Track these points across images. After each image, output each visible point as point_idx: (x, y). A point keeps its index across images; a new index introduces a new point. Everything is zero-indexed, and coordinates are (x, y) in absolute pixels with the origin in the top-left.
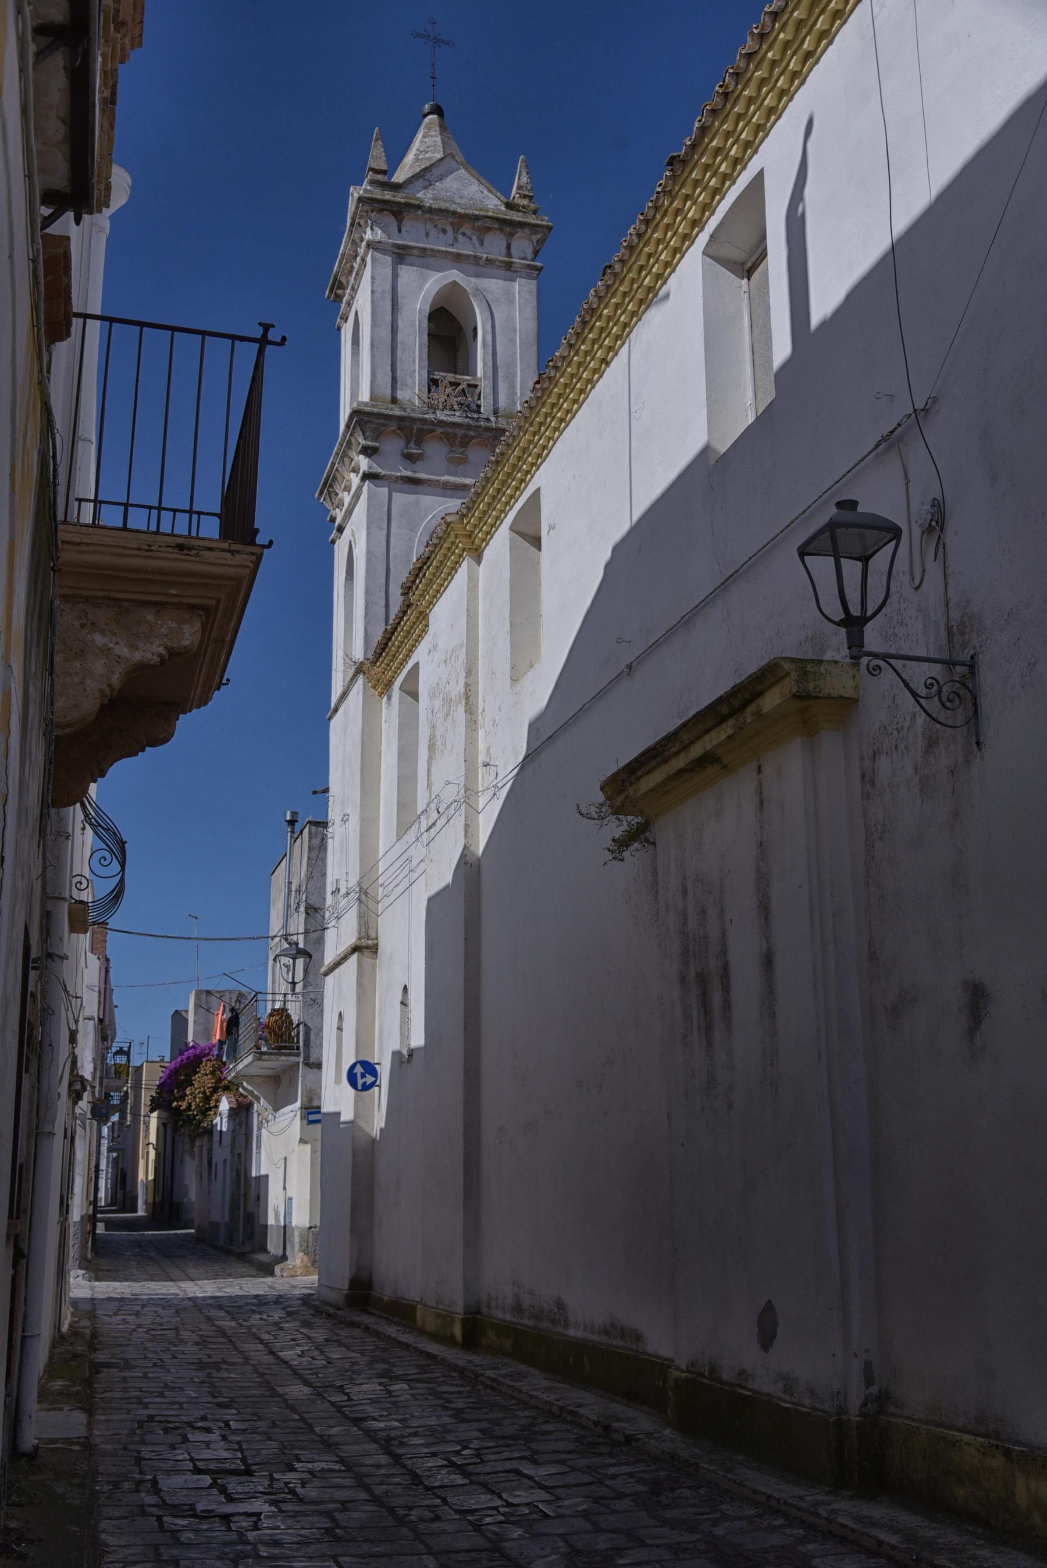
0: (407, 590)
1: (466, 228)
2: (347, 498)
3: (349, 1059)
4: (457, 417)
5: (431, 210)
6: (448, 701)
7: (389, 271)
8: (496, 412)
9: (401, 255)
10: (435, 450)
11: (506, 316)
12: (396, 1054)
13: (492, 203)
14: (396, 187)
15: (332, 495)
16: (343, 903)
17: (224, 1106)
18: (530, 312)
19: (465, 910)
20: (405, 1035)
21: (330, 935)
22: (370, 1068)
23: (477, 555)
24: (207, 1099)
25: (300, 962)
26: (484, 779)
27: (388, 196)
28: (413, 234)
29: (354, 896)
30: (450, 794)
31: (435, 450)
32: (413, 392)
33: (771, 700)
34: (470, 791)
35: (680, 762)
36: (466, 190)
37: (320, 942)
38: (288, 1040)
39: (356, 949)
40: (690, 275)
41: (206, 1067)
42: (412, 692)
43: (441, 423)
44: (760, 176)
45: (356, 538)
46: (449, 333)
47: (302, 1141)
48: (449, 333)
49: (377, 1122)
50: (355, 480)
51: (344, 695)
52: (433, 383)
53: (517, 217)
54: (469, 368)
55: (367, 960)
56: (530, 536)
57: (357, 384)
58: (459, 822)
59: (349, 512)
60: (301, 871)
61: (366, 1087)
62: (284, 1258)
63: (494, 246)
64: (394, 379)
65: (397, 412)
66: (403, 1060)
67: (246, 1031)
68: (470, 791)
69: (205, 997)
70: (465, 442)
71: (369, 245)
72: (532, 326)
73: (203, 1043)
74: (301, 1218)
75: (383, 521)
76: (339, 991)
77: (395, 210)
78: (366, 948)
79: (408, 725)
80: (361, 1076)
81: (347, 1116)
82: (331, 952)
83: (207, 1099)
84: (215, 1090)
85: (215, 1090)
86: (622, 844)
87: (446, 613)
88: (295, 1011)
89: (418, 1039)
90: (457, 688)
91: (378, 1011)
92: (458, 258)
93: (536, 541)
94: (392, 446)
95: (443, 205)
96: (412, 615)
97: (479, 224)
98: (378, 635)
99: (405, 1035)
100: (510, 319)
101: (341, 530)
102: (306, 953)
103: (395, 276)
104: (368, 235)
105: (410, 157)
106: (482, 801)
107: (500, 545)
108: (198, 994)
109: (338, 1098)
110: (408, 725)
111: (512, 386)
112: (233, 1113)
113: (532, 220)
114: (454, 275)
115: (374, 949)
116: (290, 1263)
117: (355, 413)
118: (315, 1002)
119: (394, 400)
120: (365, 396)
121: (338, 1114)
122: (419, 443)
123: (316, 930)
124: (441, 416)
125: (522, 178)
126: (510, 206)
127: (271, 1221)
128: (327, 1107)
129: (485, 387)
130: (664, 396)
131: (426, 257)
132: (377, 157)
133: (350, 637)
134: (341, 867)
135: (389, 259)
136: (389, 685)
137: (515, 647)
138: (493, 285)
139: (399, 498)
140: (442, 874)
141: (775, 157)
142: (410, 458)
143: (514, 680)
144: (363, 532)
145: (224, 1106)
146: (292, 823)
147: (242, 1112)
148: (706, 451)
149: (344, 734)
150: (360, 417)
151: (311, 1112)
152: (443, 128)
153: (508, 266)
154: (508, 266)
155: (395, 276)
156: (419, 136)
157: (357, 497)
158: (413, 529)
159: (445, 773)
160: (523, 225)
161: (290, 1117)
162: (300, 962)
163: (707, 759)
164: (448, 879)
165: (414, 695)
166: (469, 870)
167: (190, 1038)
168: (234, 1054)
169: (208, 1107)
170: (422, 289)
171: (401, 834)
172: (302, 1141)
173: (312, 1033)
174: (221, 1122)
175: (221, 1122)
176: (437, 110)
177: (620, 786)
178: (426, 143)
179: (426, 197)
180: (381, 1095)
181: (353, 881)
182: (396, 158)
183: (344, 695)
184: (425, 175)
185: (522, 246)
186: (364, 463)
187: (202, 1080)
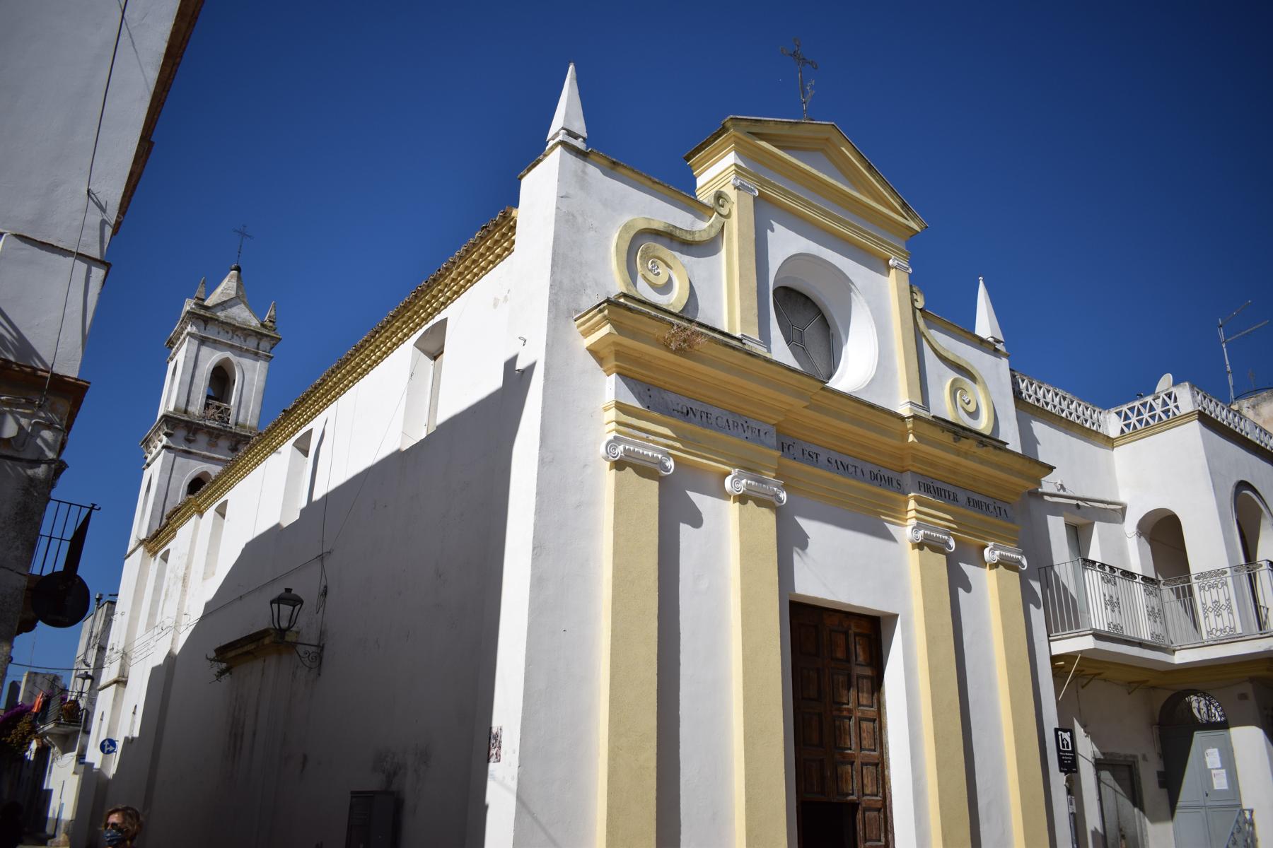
0: (169, 518)
1: (239, 333)
2: (155, 452)
3: (103, 737)
4: (215, 425)
5: (222, 322)
6: (176, 576)
7: (195, 348)
8: (236, 424)
9: (203, 341)
10: (202, 439)
11: (251, 378)
12: (126, 738)
13: (254, 323)
14: (207, 308)
15: (147, 446)
16: (114, 656)
17: (34, 746)
18: (263, 377)
19: (165, 678)
20: (132, 730)
21: (105, 671)
22: (112, 743)
23: (201, 514)
24: (24, 737)
25: (88, 682)
26: (185, 620)
27: (202, 312)
28: (211, 333)
29: (120, 655)
30: (169, 622)
31: (202, 439)
32: (197, 407)
33: (267, 641)
34: (177, 623)
35: (240, 651)
36: (242, 314)
37: (99, 677)
38: (75, 720)
39: (116, 682)
40: (288, 448)
41: (27, 718)
42: (165, 558)
43: (207, 427)
44: (311, 431)
45: (154, 472)
46: (221, 379)
47: (75, 773)
48: (221, 379)
49: (112, 771)
50: (160, 445)
51: (134, 550)
52: (207, 406)
53: (265, 332)
54: (228, 400)
55: (121, 689)
56: (221, 512)
57: (168, 402)
58: (170, 636)
59: (154, 459)
60: (99, 626)
61: (109, 752)
62: (54, 836)
63: (251, 344)
64: (188, 401)
65: (186, 418)
66: (129, 742)
67: (54, 706)
68: (177, 623)
69: (32, 676)
70: (218, 437)
71: (188, 334)
72: (262, 384)
73: (27, 704)
74: (68, 814)
75: (169, 471)
76: (105, 700)
77: (204, 317)
78: (121, 682)
79: (160, 575)
80: (107, 746)
81: (97, 766)
82: (104, 680)
83: (24, 737)
84: (30, 732)
85: (30, 732)
86: (222, 673)
87: (185, 532)
88: (82, 704)
89: (136, 734)
90: (181, 574)
91: (119, 715)
92: (232, 347)
93: (223, 516)
94: (181, 433)
95: (229, 321)
96: (168, 529)
97: (246, 332)
98: (156, 527)
99: (132, 730)
100: (253, 379)
101: (148, 465)
102: (94, 679)
103: (198, 350)
104: (189, 329)
105: (219, 290)
106: (183, 628)
107: (210, 513)
108: (30, 674)
109: (94, 756)
110: (160, 575)
111: (247, 412)
112: (38, 750)
113: (272, 334)
114: (228, 354)
115: (125, 683)
116: (57, 839)
117: (164, 416)
118: (92, 702)
119: (186, 412)
120: (171, 409)
121: (92, 764)
122: (194, 434)
123: (99, 667)
124: (208, 423)
125: (271, 312)
126: (263, 325)
127: (50, 815)
128: (88, 759)
129: (233, 411)
130: (266, 497)
131: (216, 344)
132: (200, 292)
133: (141, 527)
134: (116, 638)
135: (196, 342)
136: (155, 553)
137: (206, 565)
138: (247, 362)
139: (178, 459)
140: (160, 660)
141: (316, 425)
142: (188, 441)
143: (204, 579)
144: (159, 472)
145: (34, 746)
146: (99, 600)
147: (43, 752)
148: (278, 525)
149: (131, 566)
150: (167, 419)
151: (81, 757)
152: (239, 278)
153: (256, 354)
154: (256, 354)
155: (198, 350)
156: (226, 280)
157: (159, 454)
158: (184, 476)
159: (168, 613)
160: (267, 336)
161: (71, 757)
162: (88, 682)
163: (248, 653)
164: (161, 662)
165: (166, 561)
166: (170, 657)
167: (20, 699)
168: (44, 721)
169: (25, 744)
170: (210, 358)
171: (147, 630)
172: (75, 773)
173: (89, 714)
174: (31, 755)
175: (31, 755)
176: (238, 269)
177: (222, 652)
178: (227, 287)
179: (221, 315)
180: (115, 758)
181: (121, 648)
182: (210, 291)
183: (134, 550)
184: (223, 305)
185: (265, 344)
186: (165, 439)
187: (23, 726)
